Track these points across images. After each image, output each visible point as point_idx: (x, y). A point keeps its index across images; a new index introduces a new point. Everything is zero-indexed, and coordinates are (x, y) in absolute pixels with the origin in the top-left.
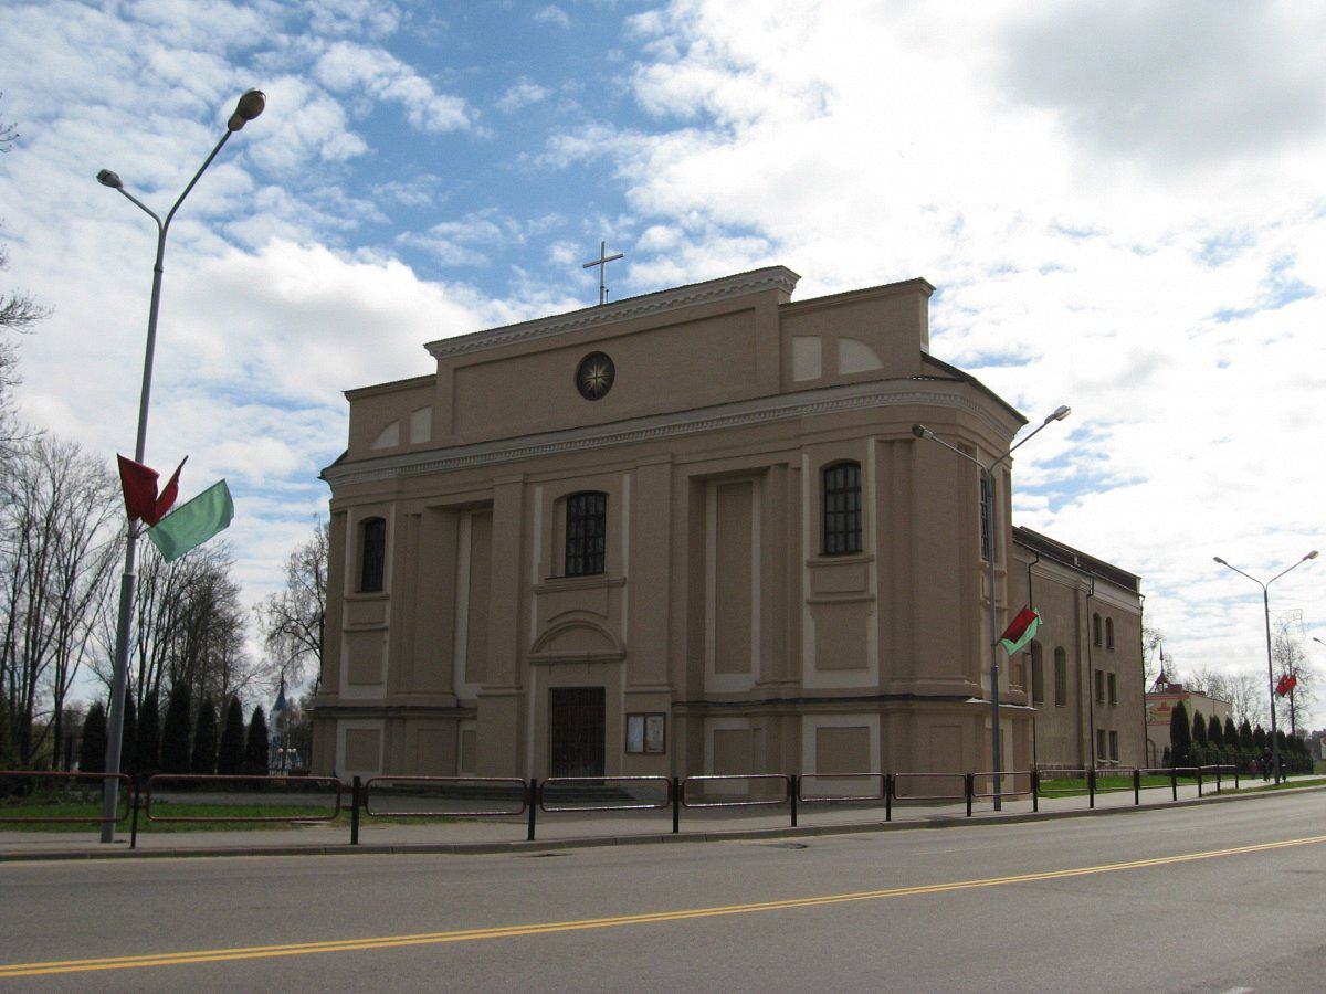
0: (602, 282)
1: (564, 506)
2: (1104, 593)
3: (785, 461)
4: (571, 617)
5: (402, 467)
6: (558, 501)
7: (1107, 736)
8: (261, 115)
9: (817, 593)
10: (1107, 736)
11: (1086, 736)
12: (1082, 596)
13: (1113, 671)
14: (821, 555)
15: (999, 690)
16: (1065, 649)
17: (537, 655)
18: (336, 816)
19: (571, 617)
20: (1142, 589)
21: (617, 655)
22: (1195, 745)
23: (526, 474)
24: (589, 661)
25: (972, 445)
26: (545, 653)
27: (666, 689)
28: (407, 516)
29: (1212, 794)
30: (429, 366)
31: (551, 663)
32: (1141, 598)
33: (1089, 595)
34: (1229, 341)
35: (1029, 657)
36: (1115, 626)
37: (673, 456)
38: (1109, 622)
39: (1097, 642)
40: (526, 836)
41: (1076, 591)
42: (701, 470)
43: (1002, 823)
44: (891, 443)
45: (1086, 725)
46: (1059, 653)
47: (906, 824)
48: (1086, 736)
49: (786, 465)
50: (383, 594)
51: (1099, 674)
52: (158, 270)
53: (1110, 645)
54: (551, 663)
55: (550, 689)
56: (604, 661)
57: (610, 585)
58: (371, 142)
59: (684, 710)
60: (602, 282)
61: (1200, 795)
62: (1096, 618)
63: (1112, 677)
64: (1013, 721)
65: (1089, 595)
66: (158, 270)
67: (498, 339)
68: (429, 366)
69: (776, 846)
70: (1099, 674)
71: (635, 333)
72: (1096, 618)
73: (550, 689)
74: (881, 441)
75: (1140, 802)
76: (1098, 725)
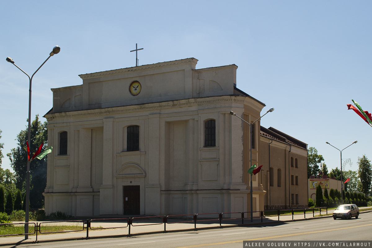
3: (194, 118)
8: (59, 53)
11: (288, 196)
14: (204, 147)
15: (253, 186)
18: (83, 230)
22: (324, 198)
25: (248, 115)
27: (159, 186)
30: (80, 82)
33: (290, 151)
35: (269, 172)
38: (296, 160)
39: (292, 166)
40: (261, 221)
42: (169, 120)
45: (288, 192)
46: (279, 170)
48: (288, 196)
49: (194, 119)
51: (292, 176)
52: (30, 91)
55: (123, 186)
62: (292, 158)
63: (297, 177)
64: (259, 195)
65: (290, 151)
66: (30, 91)
68: (79, 82)
69: (188, 233)
70: (292, 176)
71: (154, 114)
72: (292, 158)
73: (123, 186)
75: (131, 233)
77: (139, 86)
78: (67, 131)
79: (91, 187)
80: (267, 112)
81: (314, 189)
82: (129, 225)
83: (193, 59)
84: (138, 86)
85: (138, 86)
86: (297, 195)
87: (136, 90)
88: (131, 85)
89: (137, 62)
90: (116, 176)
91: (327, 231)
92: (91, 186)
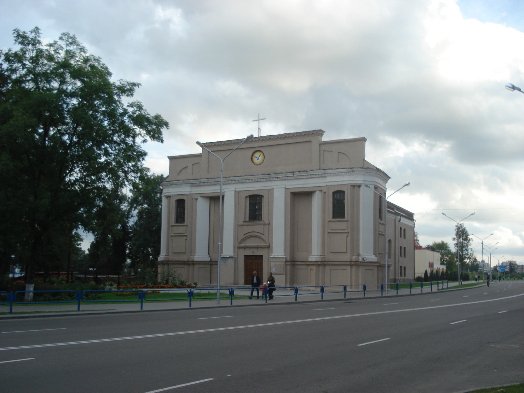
0: (259, 126)
1: (248, 200)
2: (404, 221)
3: (321, 189)
4: (250, 234)
5: (191, 184)
6: (246, 197)
7: (403, 268)
9: (244, 235)
10: (403, 268)
11: (397, 269)
12: (397, 222)
13: (405, 246)
16: (392, 240)
17: (239, 245)
19: (250, 234)
20: (415, 218)
21: (267, 246)
23: (236, 188)
24: (257, 247)
26: (243, 245)
28: (193, 199)
29: (441, 289)
30: (199, 150)
31: (245, 248)
32: (415, 221)
34: (481, 346)
36: (406, 231)
37: (285, 186)
38: (404, 230)
39: (401, 236)
41: (395, 220)
43: (401, 297)
44: (354, 186)
45: (397, 265)
47: (405, 295)
50: (185, 224)
53: (404, 237)
54: (245, 248)
56: (262, 247)
57: (264, 224)
58: (445, 272)
59: (289, 263)
60: (259, 126)
61: (438, 289)
67: (221, 144)
72: (401, 228)
74: (351, 186)
76: (401, 265)
77: (261, 155)
78: (184, 199)
79: (209, 256)
80: (404, 186)
81: (134, 222)
82: (230, 296)
83: (320, 130)
84: (260, 155)
85: (260, 155)
86: (405, 268)
87: (258, 159)
88: (252, 156)
89: (259, 132)
90: (237, 246)
91: (218, 278)
92: (209, 255)
